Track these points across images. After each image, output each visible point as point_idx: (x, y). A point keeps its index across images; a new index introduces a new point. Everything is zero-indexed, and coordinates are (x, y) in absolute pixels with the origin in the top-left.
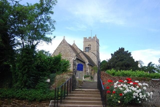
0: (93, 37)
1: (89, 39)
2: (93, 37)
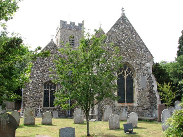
0: (79, 24)
1: (72, 26)
2: (79, 24)
